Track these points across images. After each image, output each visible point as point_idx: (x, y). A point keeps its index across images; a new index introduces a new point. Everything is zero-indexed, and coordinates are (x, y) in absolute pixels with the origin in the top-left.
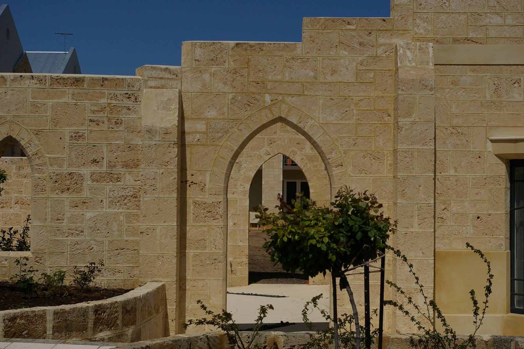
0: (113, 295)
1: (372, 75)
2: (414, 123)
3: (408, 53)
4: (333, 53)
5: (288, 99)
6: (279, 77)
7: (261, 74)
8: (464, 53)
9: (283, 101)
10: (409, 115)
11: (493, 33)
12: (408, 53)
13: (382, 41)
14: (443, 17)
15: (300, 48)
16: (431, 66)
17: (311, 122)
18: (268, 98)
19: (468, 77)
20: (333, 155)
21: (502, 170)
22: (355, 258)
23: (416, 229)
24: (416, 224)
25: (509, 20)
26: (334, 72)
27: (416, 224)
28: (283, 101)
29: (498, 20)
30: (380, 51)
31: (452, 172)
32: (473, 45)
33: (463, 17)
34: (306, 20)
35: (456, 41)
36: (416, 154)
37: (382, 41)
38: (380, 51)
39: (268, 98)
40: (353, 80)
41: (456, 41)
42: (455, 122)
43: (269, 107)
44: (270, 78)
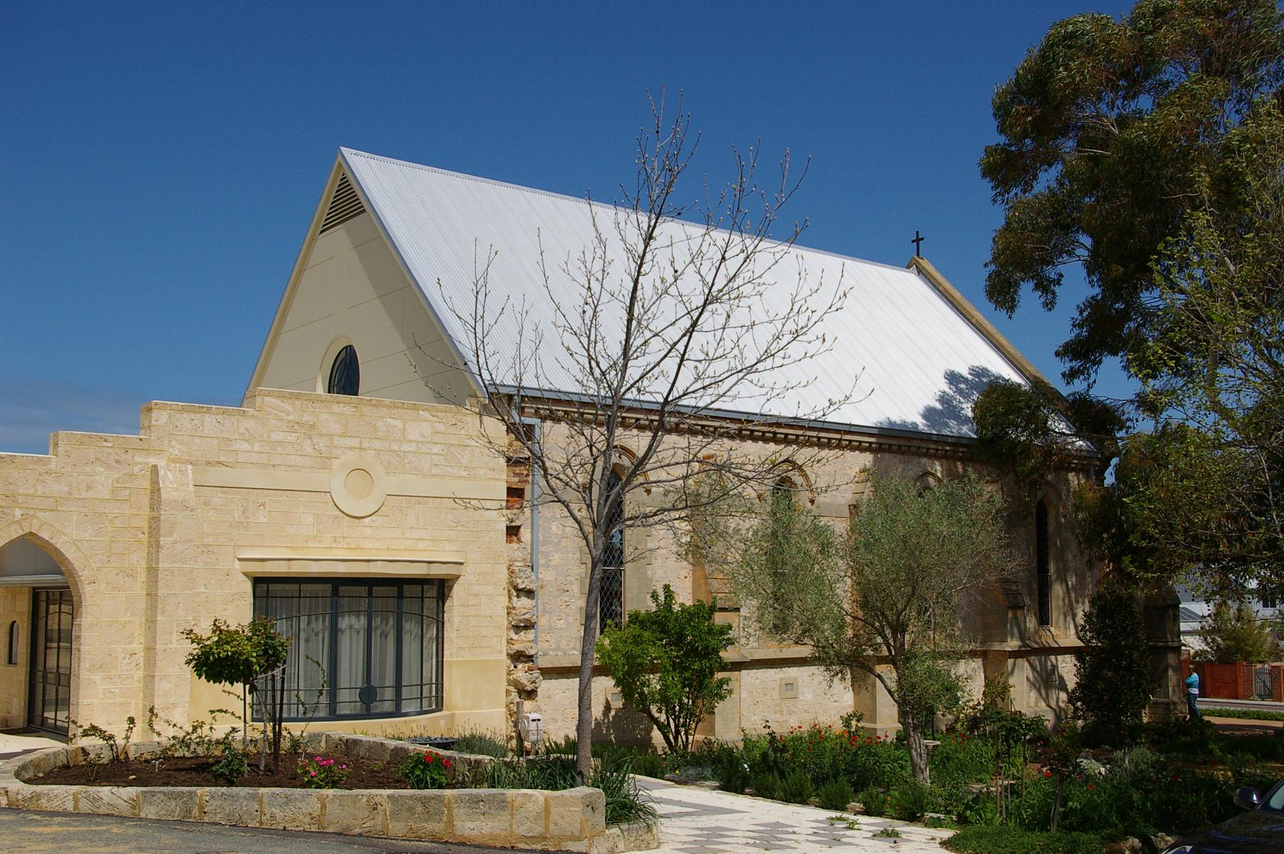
0: (1265, 719)
1: (127, 492)
2: (175, 542)
3: (169, 474)
4: (88, 469)
5: (40, 514)
6: (31, 491)
7: (11, 487)
8: (215, 476)
9: (34, 516)
10: (171, 535)
11: (242, 458)
12: (169, 474)
13: (138, 459)
14: (197, 440)
15: (54, 462)
16: (191, 488)
17: (64, 538)
18: (18, 512)
19: (218, 498)
20: (86, 572)
21: (248, 586)
22: (1085, 763)
23: (174, 645)
24: (174, 641)
25: (256, 448)
26: (89, 488)
27: (174, 641)
28: (34, 516)
29: (246, 446)
30: (136, 469)
31: (202, 589)
32: (224, 468)
33: (215, 441)
34: (62, 434)
35: (208, 463)
36: (176, 573)
37: (138, 459)
38: (136, 469)
39: (18, 512)
40: (109, 497)
41: (208, 463)
42: (206, 541)
43: (19, 522)
44: (21, 491)
